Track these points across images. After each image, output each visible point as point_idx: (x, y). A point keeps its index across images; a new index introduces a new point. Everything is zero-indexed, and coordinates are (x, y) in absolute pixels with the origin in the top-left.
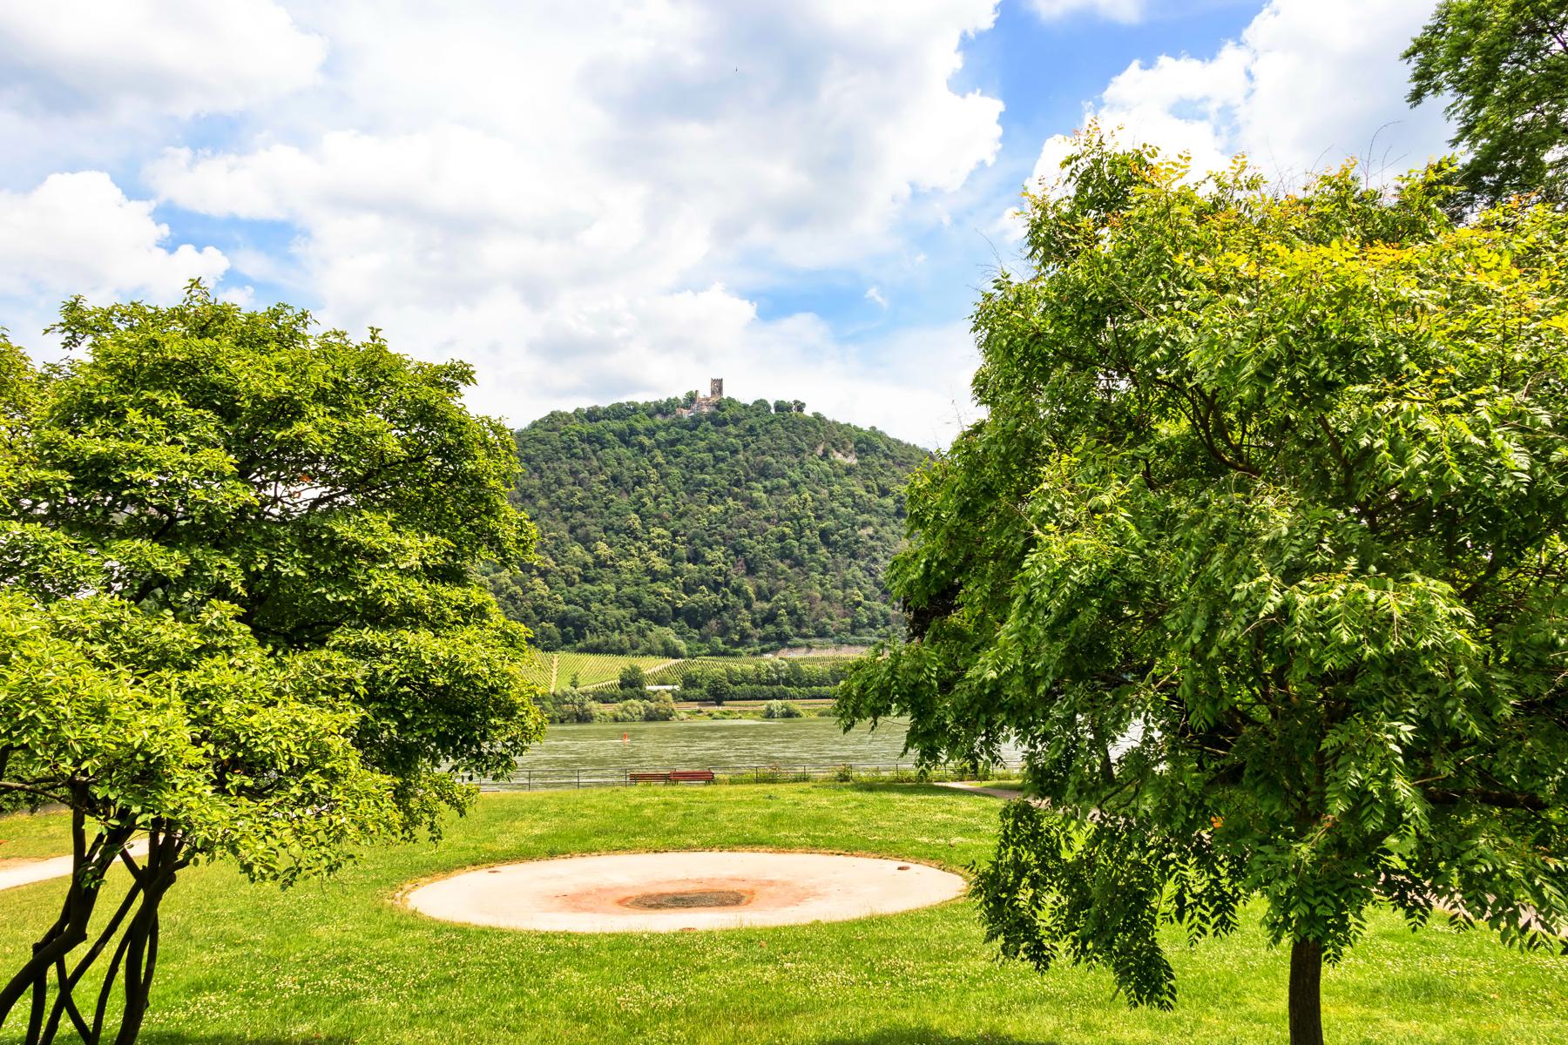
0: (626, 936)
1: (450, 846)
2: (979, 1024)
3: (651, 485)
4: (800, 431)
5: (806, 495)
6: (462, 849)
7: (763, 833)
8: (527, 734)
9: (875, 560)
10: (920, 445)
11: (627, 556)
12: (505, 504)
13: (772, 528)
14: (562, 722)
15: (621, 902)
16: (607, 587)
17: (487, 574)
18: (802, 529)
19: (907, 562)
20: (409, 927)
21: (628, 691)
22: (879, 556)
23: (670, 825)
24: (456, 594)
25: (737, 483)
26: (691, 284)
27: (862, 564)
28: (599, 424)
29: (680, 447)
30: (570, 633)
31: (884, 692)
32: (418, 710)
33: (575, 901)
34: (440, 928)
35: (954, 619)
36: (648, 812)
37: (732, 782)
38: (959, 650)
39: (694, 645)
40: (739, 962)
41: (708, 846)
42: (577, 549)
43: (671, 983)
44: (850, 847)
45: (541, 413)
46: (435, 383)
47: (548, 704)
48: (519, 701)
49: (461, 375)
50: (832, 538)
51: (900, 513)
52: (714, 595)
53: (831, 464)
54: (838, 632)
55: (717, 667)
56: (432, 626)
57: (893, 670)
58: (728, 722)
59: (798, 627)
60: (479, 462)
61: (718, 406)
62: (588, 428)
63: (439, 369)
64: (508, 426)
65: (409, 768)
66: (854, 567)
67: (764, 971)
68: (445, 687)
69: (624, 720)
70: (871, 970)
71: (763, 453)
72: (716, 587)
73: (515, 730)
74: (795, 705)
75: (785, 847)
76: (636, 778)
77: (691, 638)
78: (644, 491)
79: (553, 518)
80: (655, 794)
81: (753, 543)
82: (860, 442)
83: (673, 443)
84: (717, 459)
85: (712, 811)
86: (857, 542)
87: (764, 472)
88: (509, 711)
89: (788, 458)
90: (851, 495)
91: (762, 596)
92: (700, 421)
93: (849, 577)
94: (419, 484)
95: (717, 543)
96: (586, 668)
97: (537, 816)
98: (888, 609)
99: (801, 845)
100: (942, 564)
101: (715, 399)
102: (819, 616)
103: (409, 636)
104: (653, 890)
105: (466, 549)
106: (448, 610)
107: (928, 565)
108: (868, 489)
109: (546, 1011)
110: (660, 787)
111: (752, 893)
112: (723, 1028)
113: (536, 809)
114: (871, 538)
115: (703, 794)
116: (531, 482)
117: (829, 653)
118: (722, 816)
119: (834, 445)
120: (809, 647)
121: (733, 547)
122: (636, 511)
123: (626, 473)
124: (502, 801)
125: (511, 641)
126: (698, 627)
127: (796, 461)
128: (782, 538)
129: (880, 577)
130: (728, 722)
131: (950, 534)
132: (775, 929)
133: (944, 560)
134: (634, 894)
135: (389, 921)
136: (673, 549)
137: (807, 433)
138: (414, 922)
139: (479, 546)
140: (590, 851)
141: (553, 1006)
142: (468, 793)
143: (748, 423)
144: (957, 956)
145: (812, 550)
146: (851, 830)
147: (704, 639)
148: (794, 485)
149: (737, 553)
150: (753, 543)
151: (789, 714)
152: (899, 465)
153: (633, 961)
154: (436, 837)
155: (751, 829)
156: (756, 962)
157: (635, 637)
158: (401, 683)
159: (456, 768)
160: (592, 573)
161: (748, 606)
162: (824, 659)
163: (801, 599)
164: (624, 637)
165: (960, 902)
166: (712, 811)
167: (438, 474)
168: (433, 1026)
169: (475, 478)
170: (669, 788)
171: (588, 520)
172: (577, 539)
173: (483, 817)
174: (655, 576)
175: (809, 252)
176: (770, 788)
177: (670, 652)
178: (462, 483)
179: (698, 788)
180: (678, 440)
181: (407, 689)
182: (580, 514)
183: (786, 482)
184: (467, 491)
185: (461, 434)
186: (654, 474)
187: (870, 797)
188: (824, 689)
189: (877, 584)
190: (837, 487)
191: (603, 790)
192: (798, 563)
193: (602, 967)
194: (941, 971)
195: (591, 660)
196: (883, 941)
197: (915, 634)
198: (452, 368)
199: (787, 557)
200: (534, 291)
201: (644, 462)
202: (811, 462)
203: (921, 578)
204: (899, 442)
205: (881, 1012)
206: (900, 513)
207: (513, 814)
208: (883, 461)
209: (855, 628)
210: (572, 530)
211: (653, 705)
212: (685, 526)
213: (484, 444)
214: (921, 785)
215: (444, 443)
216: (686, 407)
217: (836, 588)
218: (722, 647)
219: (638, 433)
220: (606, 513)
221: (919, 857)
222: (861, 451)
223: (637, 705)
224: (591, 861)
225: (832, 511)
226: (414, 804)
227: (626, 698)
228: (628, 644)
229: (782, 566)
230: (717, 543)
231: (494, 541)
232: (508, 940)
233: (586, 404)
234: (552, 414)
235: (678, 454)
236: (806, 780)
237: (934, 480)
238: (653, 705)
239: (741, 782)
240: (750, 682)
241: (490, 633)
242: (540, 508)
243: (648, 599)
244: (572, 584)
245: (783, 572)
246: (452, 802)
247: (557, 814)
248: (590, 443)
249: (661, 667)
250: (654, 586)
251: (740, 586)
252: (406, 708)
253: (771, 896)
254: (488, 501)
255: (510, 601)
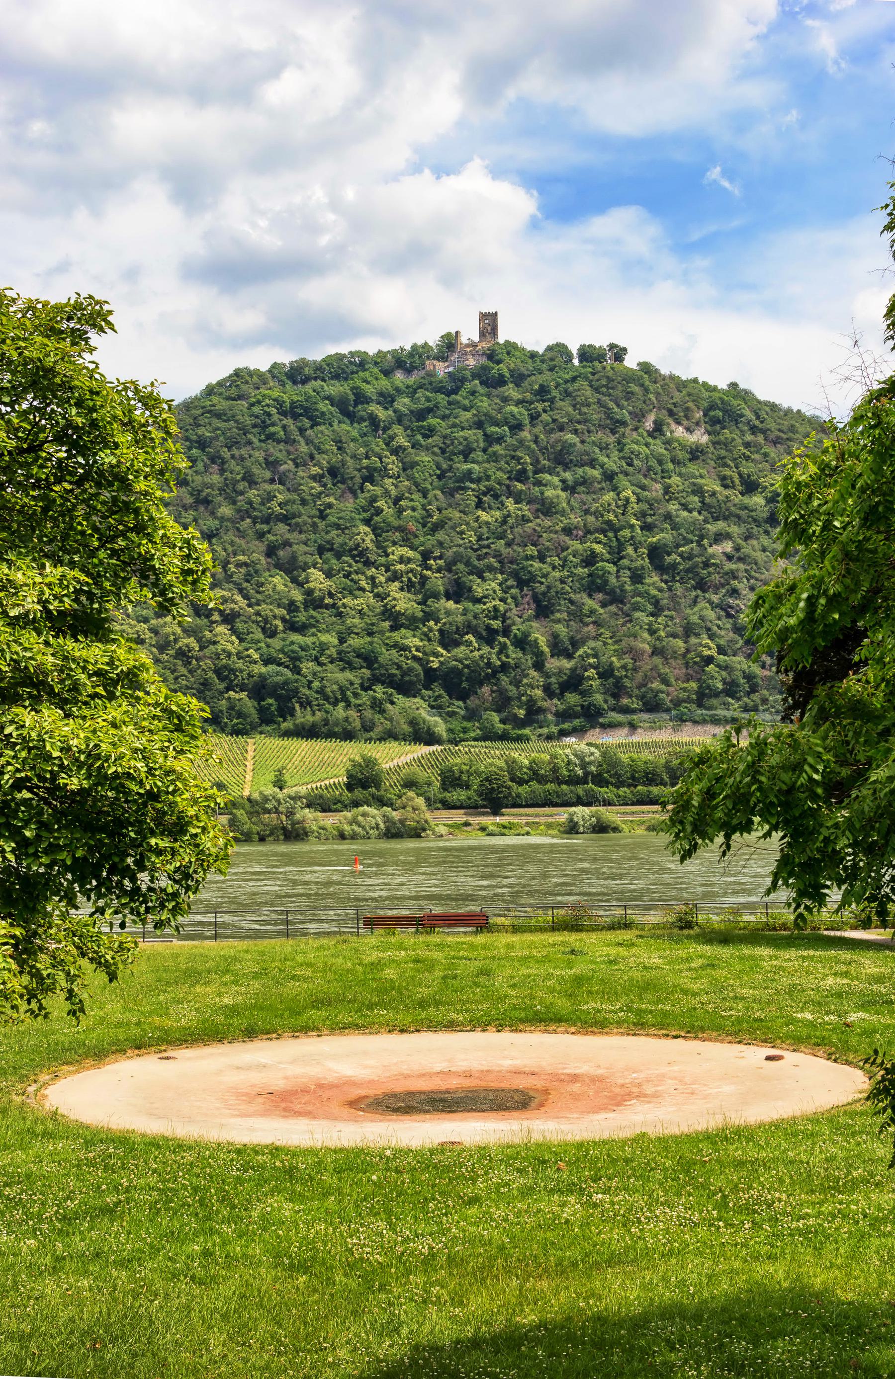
0: (359, 1152)
1: (102, 1021)
2: (883, 1283)
3: (388, 481)
4: (618, 392)
5: (628, 493)
6: (119, 1025)
7: (563, 1004)
8: (204, 860)
9: (735, 592)
10: (808, 412)
11: (354, 590)
12: (163, 516)
13: (576, 545)
14: (262, 839)
15: (353, 1104)
16: (325, 638)
17: (146, 620)
18: (621, 546)
19: (779, 598)
20: (48, 1135)
21: (359, 793)
22: (742, 586)
23: (424, 992)
24: (94, 653)
25: (521, 476)
26: (440, 163)
27: (715, 598)
28: (308, 388)
29: (432, 421)
30: (272, 707)
31: (740, 799)
32: (43, 826)
33: (285, 1101)
34: (92, 1137)
35: (852, 684)
36: (390, 973)
37: (516, 929)
38: (857, 734)
39: (456, 725)
40: (526, 1192)
41: (479, 1024)
42: (278, 581)
43: (427, 1221)
44: (694, 1027)
45: (218, 369)
46: (53, 332)
47: (240, 813)
48: (191, 812)
49: (91, 317)
50: (668, 559)
51: (772, 520)
52: (486, 649)
53: (668, 442)
54: (677, 703)
55: (491, 757)
56: (62, 703)
57: (753, 769)
58: (510, 840)
59: (616, 696)
60: (121, 452)
61: (491, 356)
62: (291, 394)
63: (59, 308)
64: (164, 396)
65: (34, 910)
66: (703, 604)
67: (564, 1204)
68: (82, 791)
69: (354, 837)
70: (723, 1205)
71: (561, 429)
72: (489, 637)
73: (186, 856)
74: (611, 814)
75: (595, 1025)
76: (372, 923)
77: (452, 714)
78: (378, 490)
79: (241, 534)
80: (401, 947)
81: (546, 568)
82: (712, 407)
83: (421, 415)
84: (490, 440)
85: (486, 972)
86: (706, 565)
87: (562, 459)
88: (178, 828)
89: (600, 436)
90: (698, 491)
91: (559, 649)
92: (463, 380)
93: (695, 619)
94: (34, 487)
95: (490, 568)
96: (297, 760)
97: (227, 978)
98: (756, 669)
99: (619, 1023)
100: (834, 601)
101: (485, 345)
102: (647, 679)
103: (28, 718)
104: (400, 1087)
105: (107, 584)
106: (83, 677)
107: (811, 602)
108: (726, 483)
109: (245, 1256)
110: (407, 936)
111: (546, 1092)
112: (502, 1284)
113: (226, 967)
114: (729, 558)
115: (472, 946)
116: (207, 479)
117: (664, 736)
118: (500, 981)
119: (671, 413)
120: (633, 727)
121: (515, 575)
122: (367, 522)
123: (350, 462)
124: (177, 956)
125: (178, 724)
126: (463, 697)
127: (612, 439)
128: (590, 560)
129: (744, 619)
130: (510, 840)
131: (847, 555)
132: (580, 1145)
133: (836, 595)
134: (371, 1092)
135: (19, 1126)
136: (424, 579)
137: (629, 395)
138: (55, 1127)
139: (126, 579)
140: (305, 1030)
141: (257, 1250)
142: (121, 948)
143: (537, 381)
144: (854, 1185)
145: (637, 577)
146: (694, 1001)
147: (472, 715)
148: (609, 477)
149: (522, 584)
150: (546, 568)
151: (601, 828)
152: (775, 443)
153: (370, 1188)
154: (77, 1011)
155: (543, 998)
156: (551, 1192)
157: (368, 714)
158: (19, 785)
159: (101, 911)
160: (302, 617)
161: (539, 666)
162: (656, 745)
163: (620, 654)
164: (353, 713)
165: (858, 1107)
166: (487, 973)
167: (62, 471)
168: (86, 1273)
169: (116, 477)
170: (422, 938)
171: (294, 537)
172: (279, 566)
173: (149, 978)
174: (396, 620)
175: (624, 108)
176: (572, 938)
177: (422, 735)
178: (99, 485)
179: (463, 937)
180: (429, 410)
181: (26, 795)
182: (281, 528)
183: (596, 473)
184: (106, 495)
185: (93, 409)
186: (393, 464)
187: (725, 952)
188: (655, 790)
189: (738, 630)
190: (675, 480)
191: (325, 941)
192: (615, 598)
193: (326, 1195)
194: (826, 1208)
195: (303, 748)
196: (742, 1163)
197: (795, 707)
198: (78, 306)
199: (599, 589)
200: (190, 184)
201: (378, 444)
202: (635, 442)
203: (801, 622)
204: (774, 407)
205: (737, 1265)
206: (772, 520)
207: (193, 975)
208: (749, 437)
209: (703, 697)
210: (271, 552)
211: (396, 815)
212: (441, 544)
213: (129, 424)
214: (800, 935)
215: (70, 424)
216: (441, 358)
217: (674, 636)
218: (500, 727)
219: (367, 401)
220: (322, 525)
221: (797, 1042)
222: (715, 421)
223: (374, 814)
224: (309, 1045)
225: (668, 517)
226: (43, 963)
227: (356, 804)
228: (357, 724)
229: (590, 603)
230: (490, 568)
231: (147, 572)
232: (189, 1157)
233: (286, 358)
234: (237, 373)
235: (429, 432)
236: (626, 925)
237: (824, 467)
238: (396, 815)
239: (529, 929)
240: (541, 779)
241: (144, 711)
242: (222, 519)
243: (387, 656)
244: (273, 634)
245: (593, 612)
246: (98, 961)
247: (256, 976)
248: (295, 417)
249: (410, 757)
250: (396, 636)
251: (526, 635)
252: (27, 823)
253: (575, 1097)
254: (137, 511)
255: (177, 660)
